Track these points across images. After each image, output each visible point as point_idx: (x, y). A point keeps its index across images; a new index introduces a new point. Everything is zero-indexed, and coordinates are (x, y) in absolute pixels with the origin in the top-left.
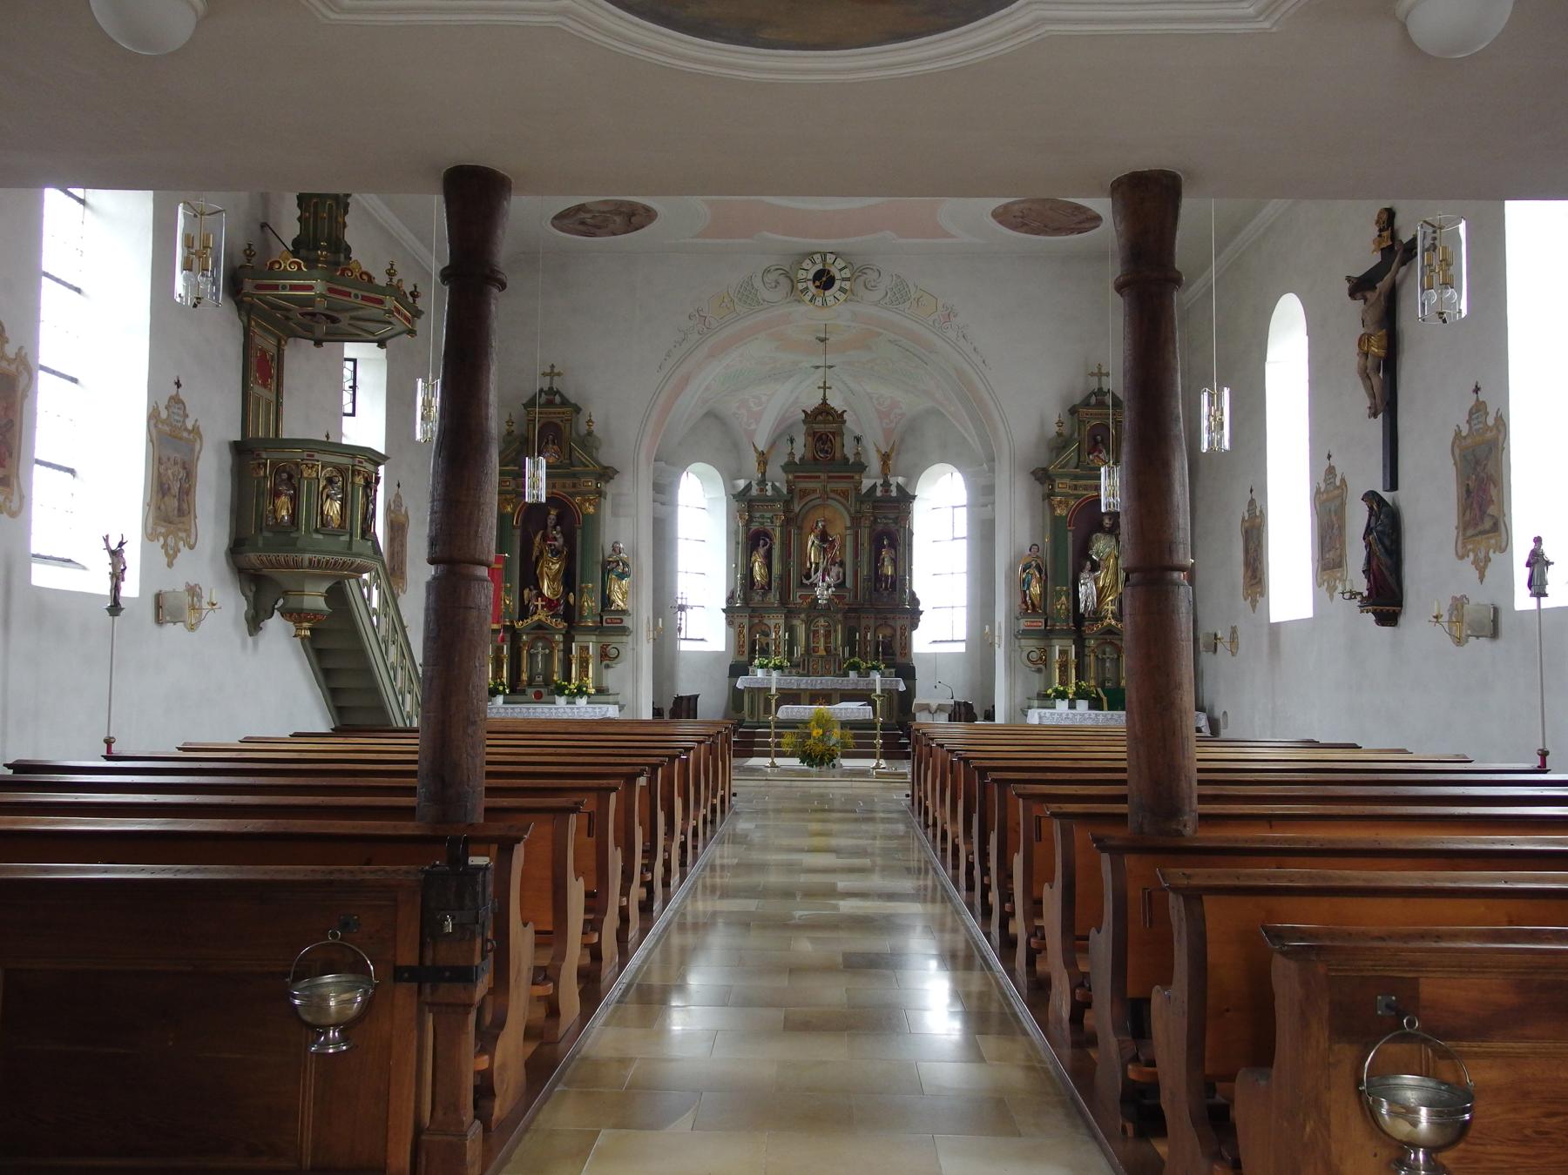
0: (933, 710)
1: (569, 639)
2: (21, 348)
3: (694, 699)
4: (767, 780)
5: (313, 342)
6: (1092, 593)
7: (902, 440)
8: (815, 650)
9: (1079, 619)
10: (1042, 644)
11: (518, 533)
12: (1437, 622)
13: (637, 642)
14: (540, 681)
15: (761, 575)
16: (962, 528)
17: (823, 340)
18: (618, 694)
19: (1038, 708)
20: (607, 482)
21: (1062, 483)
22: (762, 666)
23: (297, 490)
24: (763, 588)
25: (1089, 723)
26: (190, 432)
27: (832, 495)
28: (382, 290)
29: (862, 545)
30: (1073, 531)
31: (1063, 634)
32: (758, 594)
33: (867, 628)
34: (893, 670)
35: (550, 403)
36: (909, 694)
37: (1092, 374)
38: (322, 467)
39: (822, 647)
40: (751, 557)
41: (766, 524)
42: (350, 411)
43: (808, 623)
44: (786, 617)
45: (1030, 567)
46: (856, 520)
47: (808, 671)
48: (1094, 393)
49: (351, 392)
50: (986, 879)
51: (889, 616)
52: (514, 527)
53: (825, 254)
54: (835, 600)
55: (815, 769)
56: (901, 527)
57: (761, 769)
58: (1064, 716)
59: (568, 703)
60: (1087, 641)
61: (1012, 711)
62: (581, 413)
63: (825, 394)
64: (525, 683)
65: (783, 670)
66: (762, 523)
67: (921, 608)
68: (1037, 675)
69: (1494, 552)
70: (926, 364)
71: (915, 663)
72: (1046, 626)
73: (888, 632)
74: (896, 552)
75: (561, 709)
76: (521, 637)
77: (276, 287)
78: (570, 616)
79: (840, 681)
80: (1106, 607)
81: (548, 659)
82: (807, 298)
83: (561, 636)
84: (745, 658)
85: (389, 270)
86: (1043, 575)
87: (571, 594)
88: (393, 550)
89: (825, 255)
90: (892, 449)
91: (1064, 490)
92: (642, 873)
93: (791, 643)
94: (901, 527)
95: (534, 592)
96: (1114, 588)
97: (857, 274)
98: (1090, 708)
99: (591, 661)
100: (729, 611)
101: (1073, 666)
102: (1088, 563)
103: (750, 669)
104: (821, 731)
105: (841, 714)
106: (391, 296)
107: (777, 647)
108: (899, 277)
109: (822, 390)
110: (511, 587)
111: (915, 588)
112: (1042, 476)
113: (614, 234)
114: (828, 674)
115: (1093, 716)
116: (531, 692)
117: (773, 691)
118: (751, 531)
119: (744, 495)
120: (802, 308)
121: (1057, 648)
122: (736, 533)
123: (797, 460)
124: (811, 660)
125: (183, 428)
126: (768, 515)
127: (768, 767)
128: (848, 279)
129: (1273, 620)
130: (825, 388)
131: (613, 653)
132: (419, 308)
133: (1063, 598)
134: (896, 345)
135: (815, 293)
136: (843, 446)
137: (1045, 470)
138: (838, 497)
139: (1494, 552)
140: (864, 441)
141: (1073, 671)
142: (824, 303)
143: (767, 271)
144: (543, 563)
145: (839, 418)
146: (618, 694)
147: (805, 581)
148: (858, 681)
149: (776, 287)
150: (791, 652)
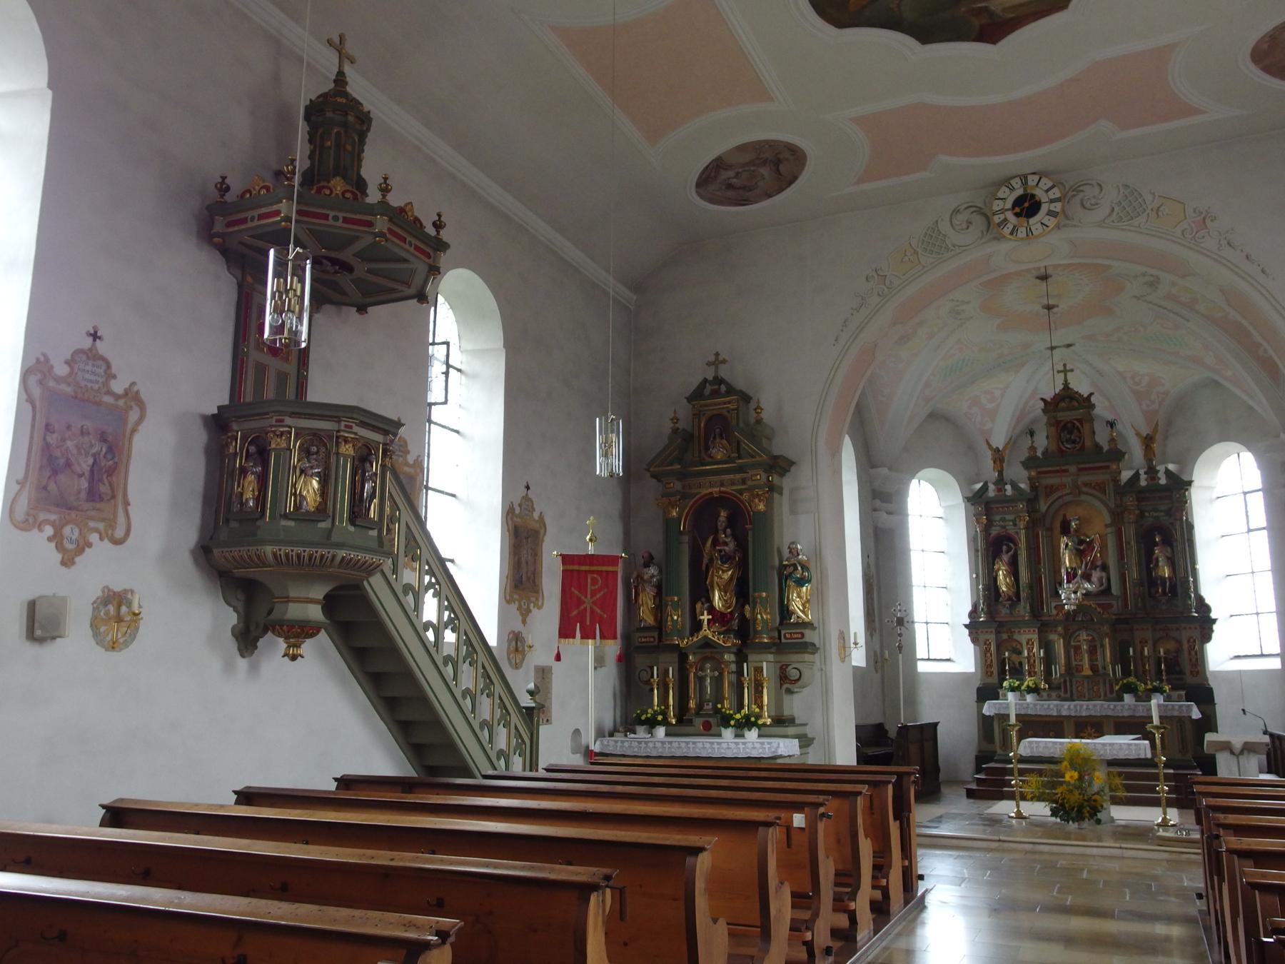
0: (1237, 751)
1: (741, 658)
2: (419, 456)
3: (934, 726)
4: (1000, 841)
5: (355, 309)
8: (1079, 669)
11: (686, 539)
13: (825, 660)
14: (708, 710)
15: (1007, 585)
16: (1259, 516)
22: (1012, 689)
23: (265, 463)
26: (117, 397)
27: (1084, 489)
28: (371, 210)
32: (1005, 606)
33: (1144, 642)
34: (1183, 693)
36: (1208, 723)
38: (296, 435)
39: (1086, 666)
40: (994, 564)
43: (1067, 637)
44: (1040, 632)
46: (1117, 517)
47: (1072, 694)
49: (444, 379)
52: (681, 533)
53: (1025, 177)
54: (1099, 610)
55: (1072, 826)
56: (1176, 520)
59: (737, 736)
63: (1066, 380)
64: (693, 712)
65: (1038, 694)
66: (1004, 527)
67: (1213, 615)
70: (1188, 321)
71: (1212, 683)
73: (1172, 645)
74: (1172, 549)
76: (688, 657)
77: (244, 221)
78: (745, 632)
79: (1112, 707)
81: (718, 682)
82: (1007, 231)
84: (994, 680)
89: (1026, 178)
90: (1156, 430)
93: (1049, 660)
94: (1176, 520)
97: (1070, 194)
99: (765, 684)
100: (974, 628)
104: (1076, 775)
105: (1106, 750)
106: (382, 215)
107: (1032, 666)
108: (1128, 186)
109: (1062, 375)
110: (679, 600)
113: (770, 196)
114: (1097, 697)
116: (698, 722)
117: (1013, 720)
118: (992, 535)
119: (980, 497)
120: (1005, 247)
123: (1039, 454)
124: (1074, 680)
125: (105, 389)
126: (1010, 517)
127: (1012, 817)
131: (794, 674)
132: (444, 240)
134: (1145, 301)
140: (1119, 427)
143: (956, 211)
144: (713, 572)
145: (1086, 403)
148: (1136, 706)
149: (968, 227)
150: (1048, 673)
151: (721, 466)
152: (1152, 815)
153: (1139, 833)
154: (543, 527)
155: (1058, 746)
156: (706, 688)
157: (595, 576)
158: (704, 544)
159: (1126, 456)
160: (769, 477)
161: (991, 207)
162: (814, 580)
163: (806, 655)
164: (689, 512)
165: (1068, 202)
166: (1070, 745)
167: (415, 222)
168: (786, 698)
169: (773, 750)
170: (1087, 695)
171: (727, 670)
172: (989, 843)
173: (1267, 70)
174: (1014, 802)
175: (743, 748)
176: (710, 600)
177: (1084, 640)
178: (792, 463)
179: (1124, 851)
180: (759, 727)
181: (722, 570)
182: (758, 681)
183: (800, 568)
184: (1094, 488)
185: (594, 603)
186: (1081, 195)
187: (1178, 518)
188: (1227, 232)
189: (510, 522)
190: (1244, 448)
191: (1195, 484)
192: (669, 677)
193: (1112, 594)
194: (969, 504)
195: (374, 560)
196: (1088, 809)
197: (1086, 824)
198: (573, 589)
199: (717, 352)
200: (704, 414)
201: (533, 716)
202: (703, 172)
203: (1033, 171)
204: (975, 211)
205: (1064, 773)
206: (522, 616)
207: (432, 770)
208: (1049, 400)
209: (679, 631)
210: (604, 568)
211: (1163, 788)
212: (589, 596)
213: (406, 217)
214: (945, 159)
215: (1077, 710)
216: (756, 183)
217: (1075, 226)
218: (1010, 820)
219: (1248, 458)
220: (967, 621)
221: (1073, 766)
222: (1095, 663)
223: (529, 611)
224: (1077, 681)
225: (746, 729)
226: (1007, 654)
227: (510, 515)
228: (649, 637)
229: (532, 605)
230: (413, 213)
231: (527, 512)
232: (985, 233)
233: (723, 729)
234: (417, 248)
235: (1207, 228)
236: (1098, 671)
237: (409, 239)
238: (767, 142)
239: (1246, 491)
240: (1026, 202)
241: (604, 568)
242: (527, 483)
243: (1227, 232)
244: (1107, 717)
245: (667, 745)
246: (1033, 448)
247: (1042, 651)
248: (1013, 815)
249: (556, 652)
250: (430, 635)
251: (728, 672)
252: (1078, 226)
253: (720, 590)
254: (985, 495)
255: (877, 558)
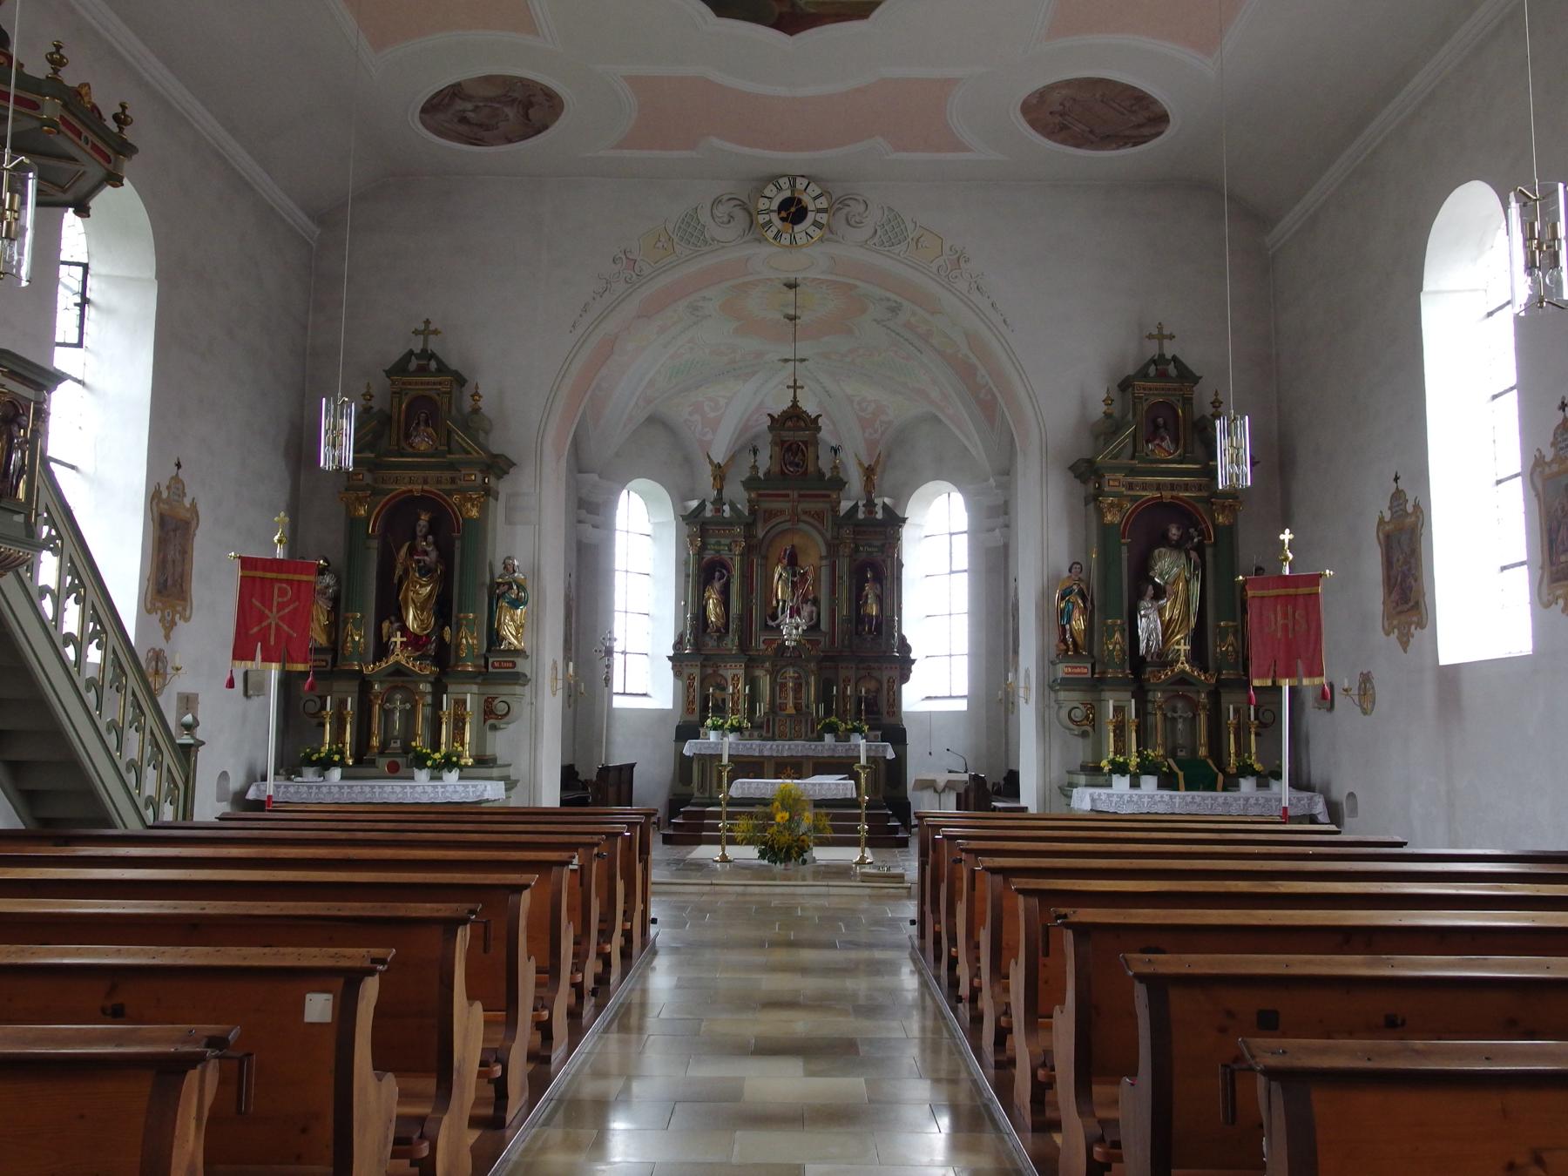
1: (439, 688)
4: (711, 884)
6: (1156, 628)
7: (889, 456)
8: (783, 707)
9: (1137, 662)
10: (1088, 697)
11: (374, 544)
12: (1348, 695)
13: (536, 693)
14: (395, 749)
15: (717, 615)
16: (962, 559)
17: (793, 318)
18: (510, 765)
19: (1086, 786)
20: (499, 477)
21: (1114, 480)
22: (715, 728)
24: (718, 630)
25: (1161, 808)
27: (804, 517)
29: (841, 578)
30: (1128, 545)
31: (1118, 684)
32: (712, 637)
33: (847, 681)
34: (879, 733)
35: (422, 370)
36: (900, 761)
37: (1150, 337)
39: (791, 704)
40: (704, 592)
41: (722, 552)
42: (75, 341)
43: (774, 673)
45: (1071, 593)
46: (833, 549)
48: (1153, 361)
49: (78, 312)
50: (937, 926)
51: (873, 665)
55: (779, 867)
56: (888, 557)
57: (708, 865)
58: (1126, 798)
59: (432, 778)
60: (1151, 694)
61: (1047, 793)
62: (466, 385)
63: (795, 397)
64: (376, 750)
65: (741, 733)
66: (718, 551)
67: (913, 656)
68: (1080, 740)
69: (1416, 629)
70: (921, 353)
71: (906, 724)
72: (1093, 673)
73: (872, 685)
75: (422, 788)
76: (372, 687)
78: (443, 659)
79: (813, 747)
80: (1177, 647)
81: (409, 716)
82: (770, 234)
83: (428, 685)
84: (696, 717)
85: (51, 54)
86: (1089, 604)
87: (447, 628)
88: (165, 557)
90: (877, 462)
91: (1116, 489)
92: (598, 944)
93: (753, 699)
95: (396, 625)
96: (1185, 623)
97: (836, 206)
98: (1161, 786)
99: (468, 719)
100: (677, 660)
101: (1134, 728)
102: (1150, 587)
103: (702, 731)
104: (787, 815)
106: (53, 97)
107: (735, 703)
108: (893, 211)
110: (362, 617)
111: (905, 632)
112: (1085, 472)
113: (510, 141)
114: (798, 737)
115: (1166, 799)
116: (383, 763)
117: (725, 760)
118: (705, 560)
120: (764, 251)
121: (1111, 703)
122: (687, 563)
123: (761, 475)
124: (777, 719)
126: (724, 541)
127: (717, 861)
128: (824, 211)
129: (1445, 658)
130: (795, 387)
131: (502, 708)
133: (1117, 635)
134: (884, 326)
135: (780, 227)
136: (818, 458)
137: (1090, 462)
138: (811, 520)
139: (1416, 629)
140: (842, 455)
141: (1134, 735)
142: (793, 239)
143: (717, 202)
144: (408, 585)
145: (813, 424)
146: (510, 765)
147: (771, 623)
149: (729, 221)
150: (752, 710)
151: (426, 460)
152: (851, 855)
153: (840, 872)
154: (195, 519)
155: (769, 787)
156: (394, 722)
157: (284, 585)
158: (398, 550)
159: (847, 486)
160: (485, 478)
161: (757, 205)
162: (530, 603)
163: (517, 687)
164: (378, 514)
165: (834, 214)
166: (784, 785)
167: (93, 111)
168: (489, 734)
169: (478, 793)
170: (788, 734)
171: (421, 702)
172: (700, 887)
173: (1033, 124)
174: (720, 847)
175: (473, 792)
176: (402, 620)
177: (790, 677)
178: (512, 464)
179: (831, 888)
180: (461, 768)
181: (420, 584)
182: (458, 715)
183: (515, 587)
184: (813, 517)
185: (282, 618)
186: (847, 209)
187: (890, 554)
188: (978, 275)
189: (155, 509)
190: (954, 488)
191: (908, 521)
192: (346, 708)
193: (820, 630)
194: (684, 524)
195: (21, 554)
196: (796, 849)
197: (791, 865)
198: (254, 600)
199: (428, 320)
200: (406, 394)
201: (187, 754)
202: (433, 98)
203: (802, 174)
204: (740, 205)
205: (775, 814)
206: (165, 630)
207: (46, 822)
208: (776, 417)
209: (360, 654)
210: (297, 577)
211: (863, 827)
212: (275, 610)
213: (82, 102)
214: (716, 142)
215: (778, 750)
216: (497, 123)
217: (837, 242)
218: (715, 864)
219: (958, 499)
220: (671, 653)
221: (785, 807)
222: (799, 701)
223: (173, 623)
224: (780, 720)
225: (446, 770)
226: (711, 690)
227: (156, 500)
228: (319, 660)
229: (178, 615)
230: (90, 98)
231: (176, 498)
232: (747, 232)
233: (416, 770)
234: (95, 147)
235: (960, 269)
236: (801, 709)
237: (84, 134)
238: (521, 80)
239: (952, 531)
240: (792, 206)
241: (297, 577)
242: (178, 459)
243: (978, 275)
244: (807, 757)
245: (346, 790)
246: (755, 468)
247: (747, 688)
248: (718, 858)
249: (229, 676)
250: (70, 652)
251: (423, 705)
252: (841, 243)
253: (416, 608)
254: (701, 515)
255: (578, 577)
